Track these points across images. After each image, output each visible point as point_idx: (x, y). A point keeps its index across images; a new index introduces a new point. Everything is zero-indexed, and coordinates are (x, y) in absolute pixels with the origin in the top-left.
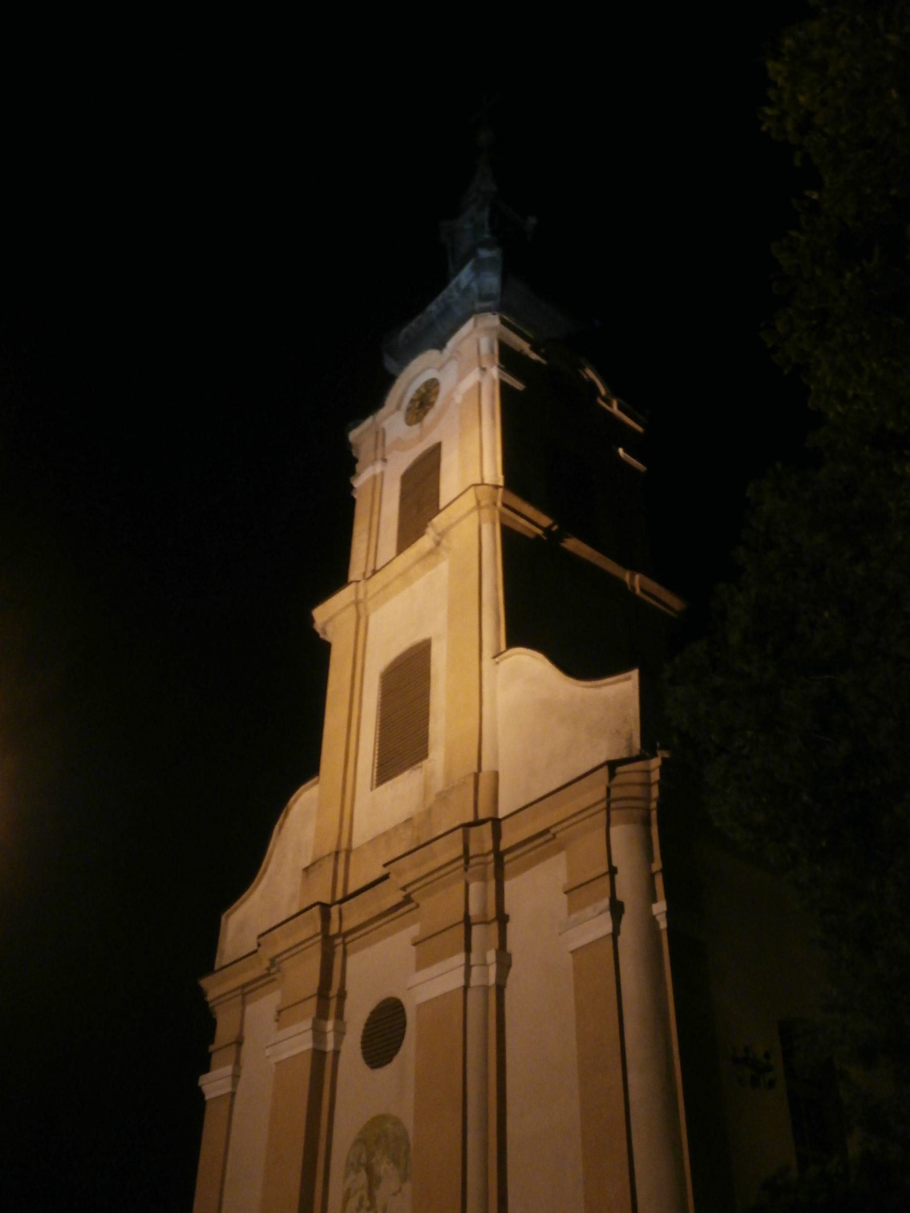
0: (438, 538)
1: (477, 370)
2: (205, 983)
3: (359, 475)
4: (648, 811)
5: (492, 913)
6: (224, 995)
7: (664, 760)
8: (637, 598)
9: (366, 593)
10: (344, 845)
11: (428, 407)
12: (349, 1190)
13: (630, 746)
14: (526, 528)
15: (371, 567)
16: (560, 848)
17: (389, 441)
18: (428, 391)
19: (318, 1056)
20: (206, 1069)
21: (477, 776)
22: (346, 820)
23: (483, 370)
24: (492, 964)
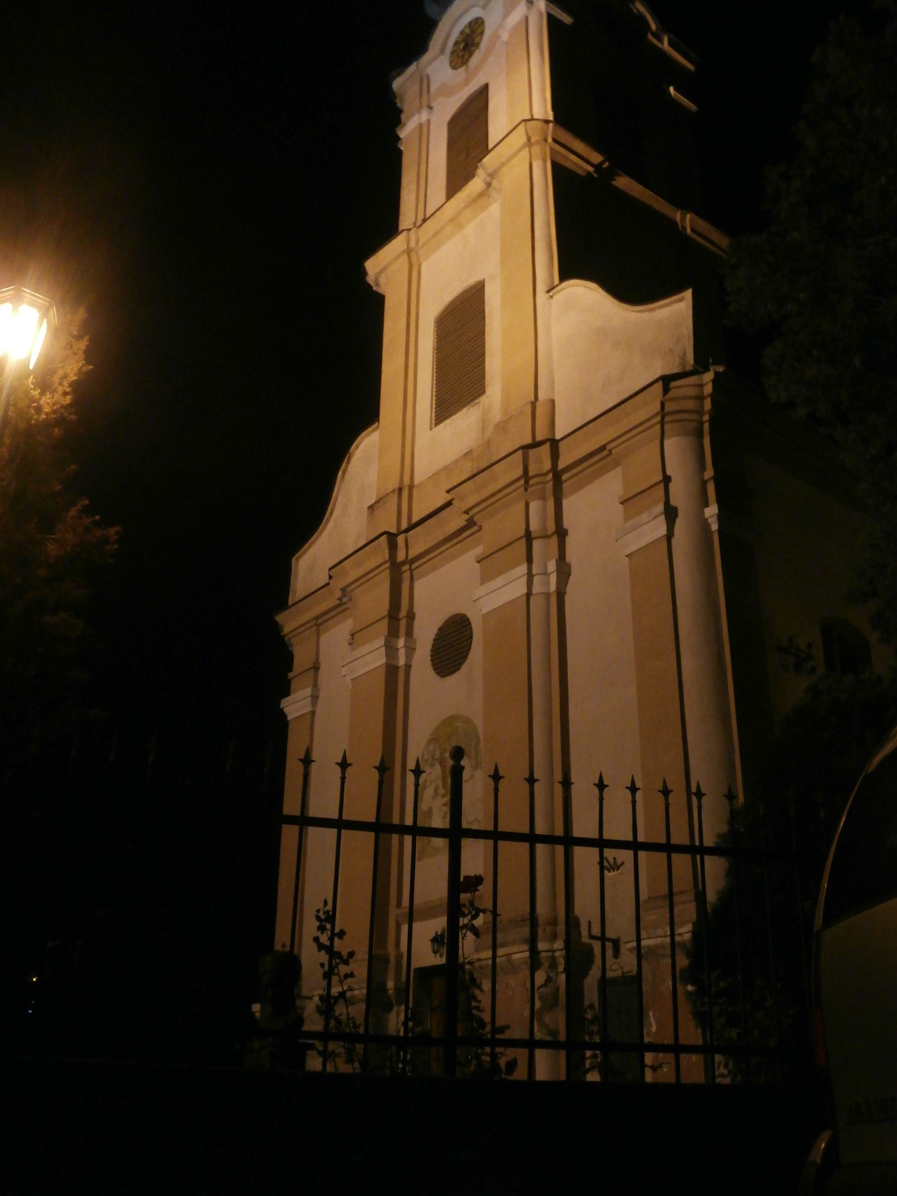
0: (488, 179)
2: (280, 618)
3: (405, 124)
4: (701, 423)
5: (551, 527)
6: (297, 628)
7: (716, 373)
9: (417, 241)
10: (406, 482)
11: (474, 48)
14: (576, 164)
15: (421, 217)
16: (617, 464)
17: (433, 89)
18: (473, 31)
19: (391, 670)
20: (287, 693)
21: (534, 405)
22: (407, 458)
24: (552, 573)
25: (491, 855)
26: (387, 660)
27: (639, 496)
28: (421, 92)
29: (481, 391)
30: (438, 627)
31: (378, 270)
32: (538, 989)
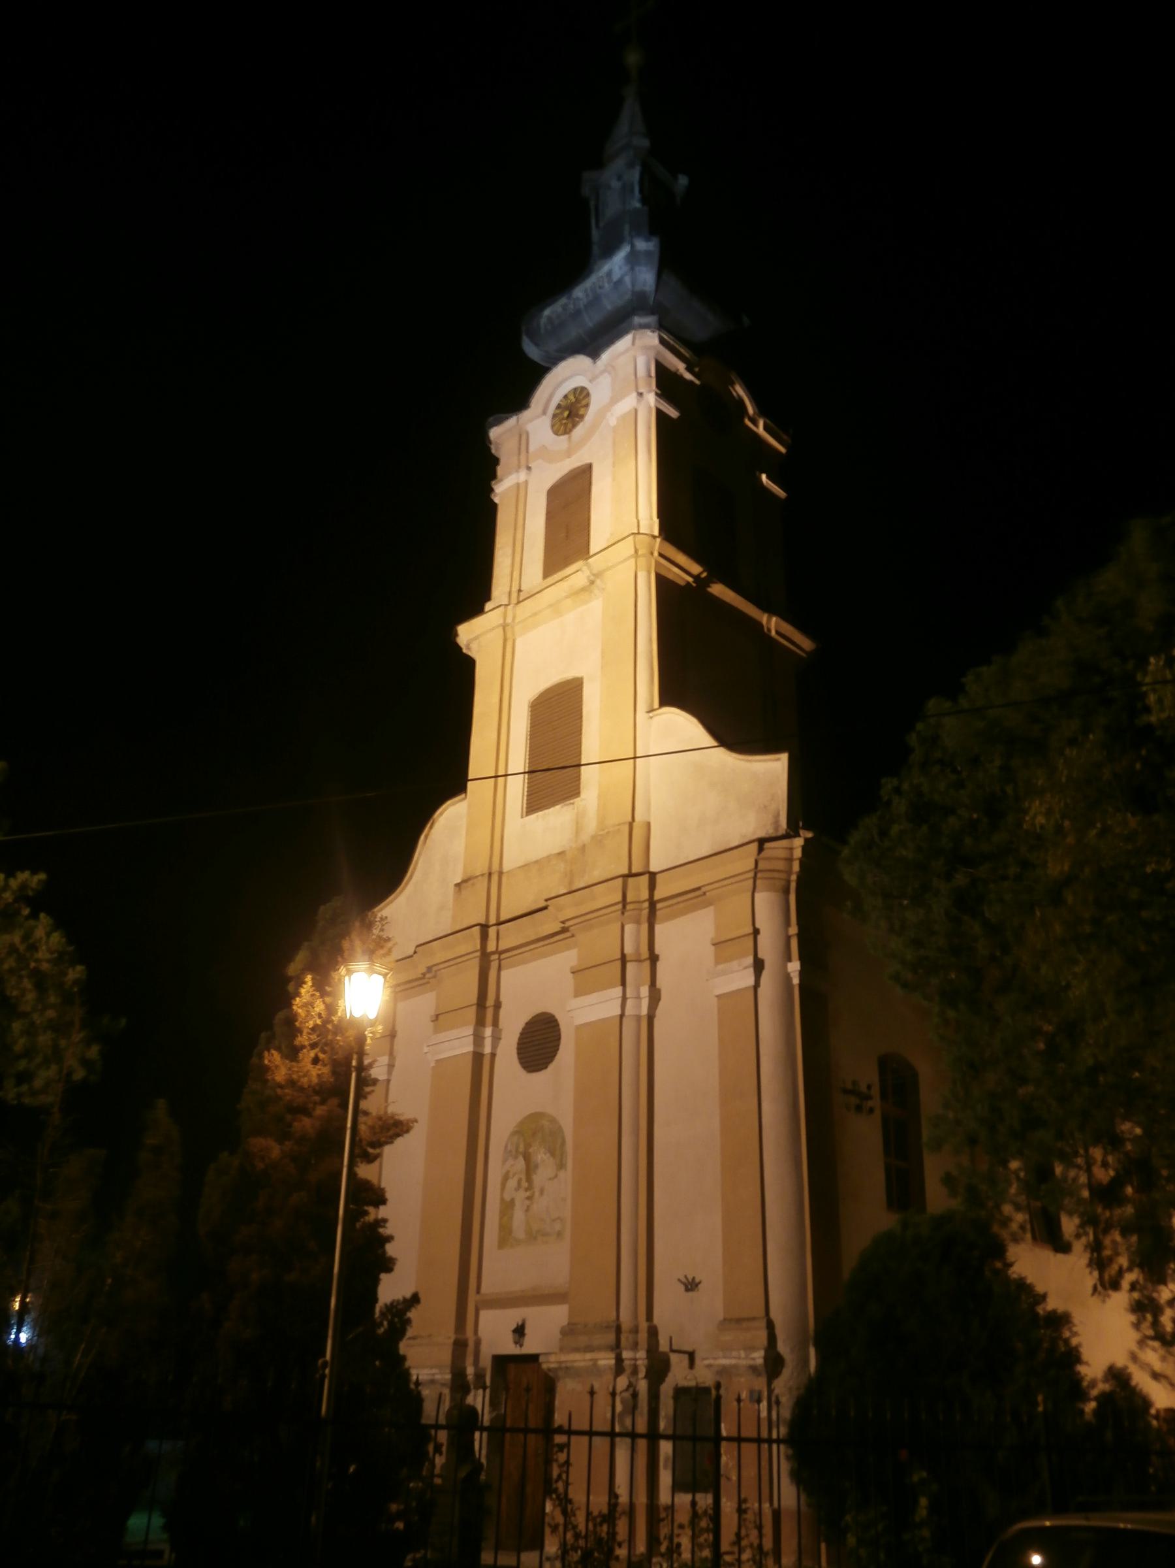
0: (592, 578)
1: (634, 394)
3: (501, 480)
4: (789, 882)
5: (645, 953)
7: (806, 840)
8: (771, 638)
9: (514, 618)
10: (495, 867)
12: (508, 1172)
13: (776, 823)
14: (678, 575)
17: (532, 448)
19: (478, 1057)
21: (631, 825)
23: (641, 394)
24: (644, 997)
25: (634, 1490)
26: (474, 1048)
27: (730, 942)
28: (519, 449)
29: (577, 793)
30: (526, 1021)
31: (472, 637)
32: (621, 1393)
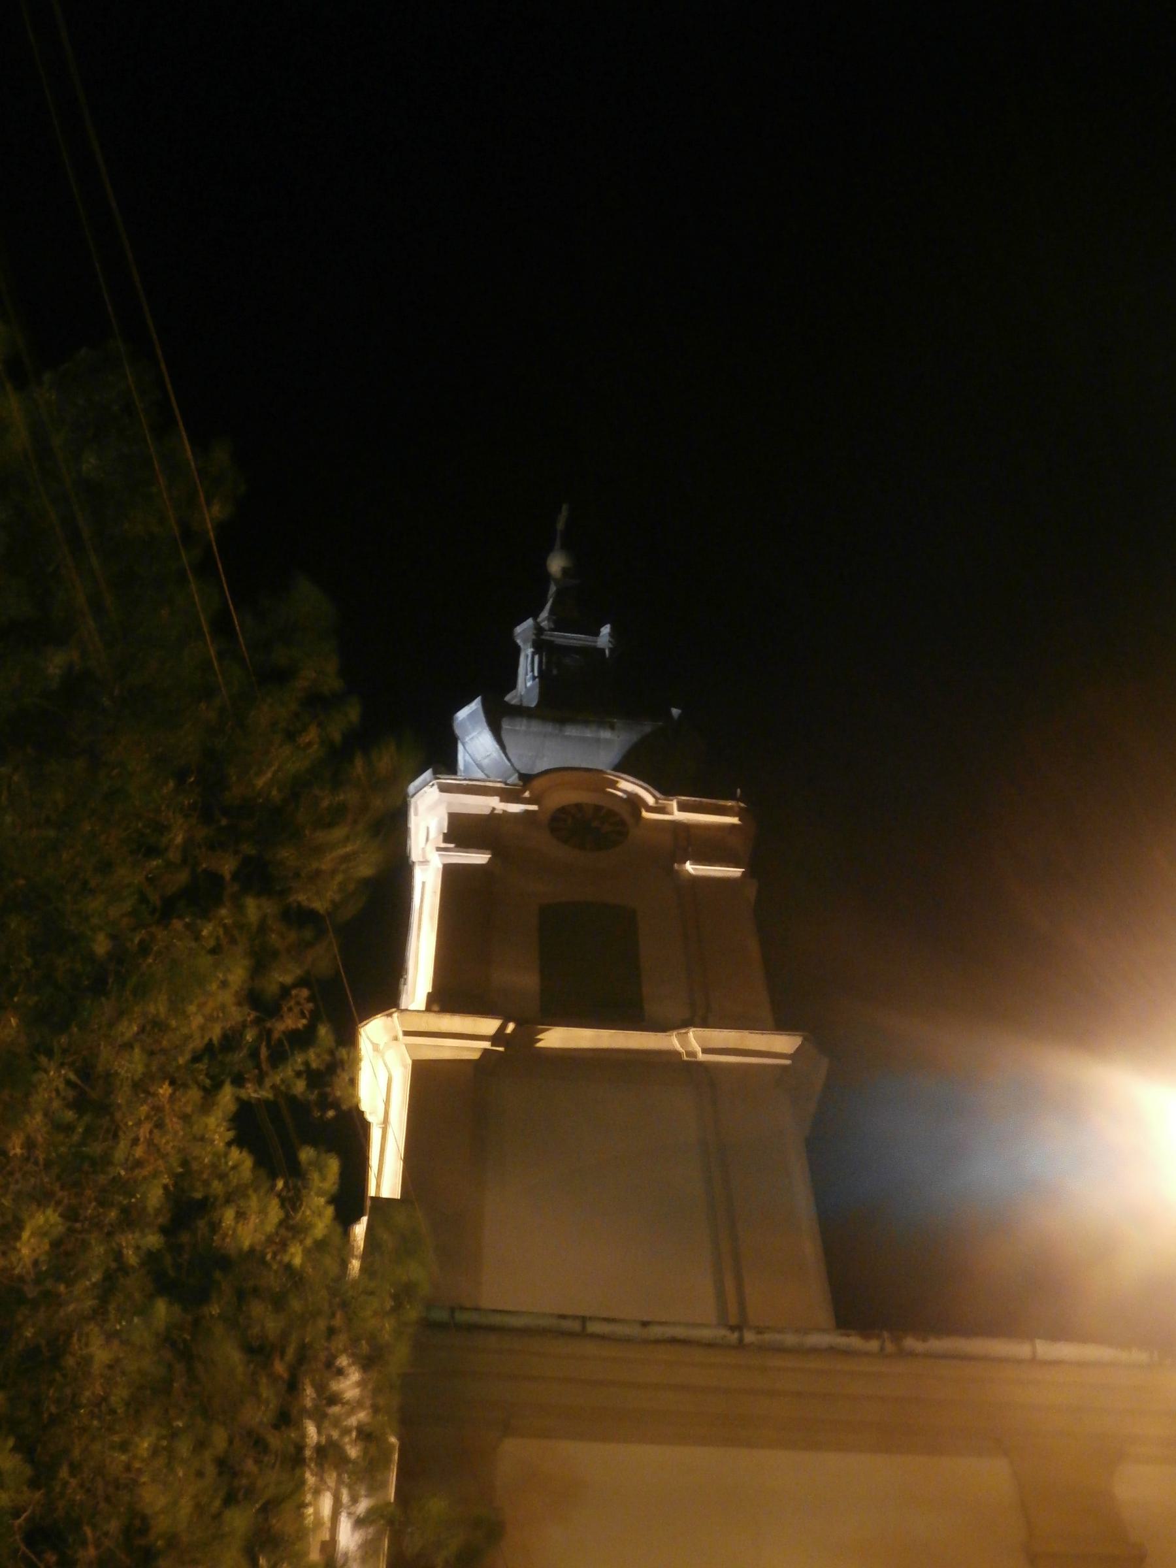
8: (700, 1064)
